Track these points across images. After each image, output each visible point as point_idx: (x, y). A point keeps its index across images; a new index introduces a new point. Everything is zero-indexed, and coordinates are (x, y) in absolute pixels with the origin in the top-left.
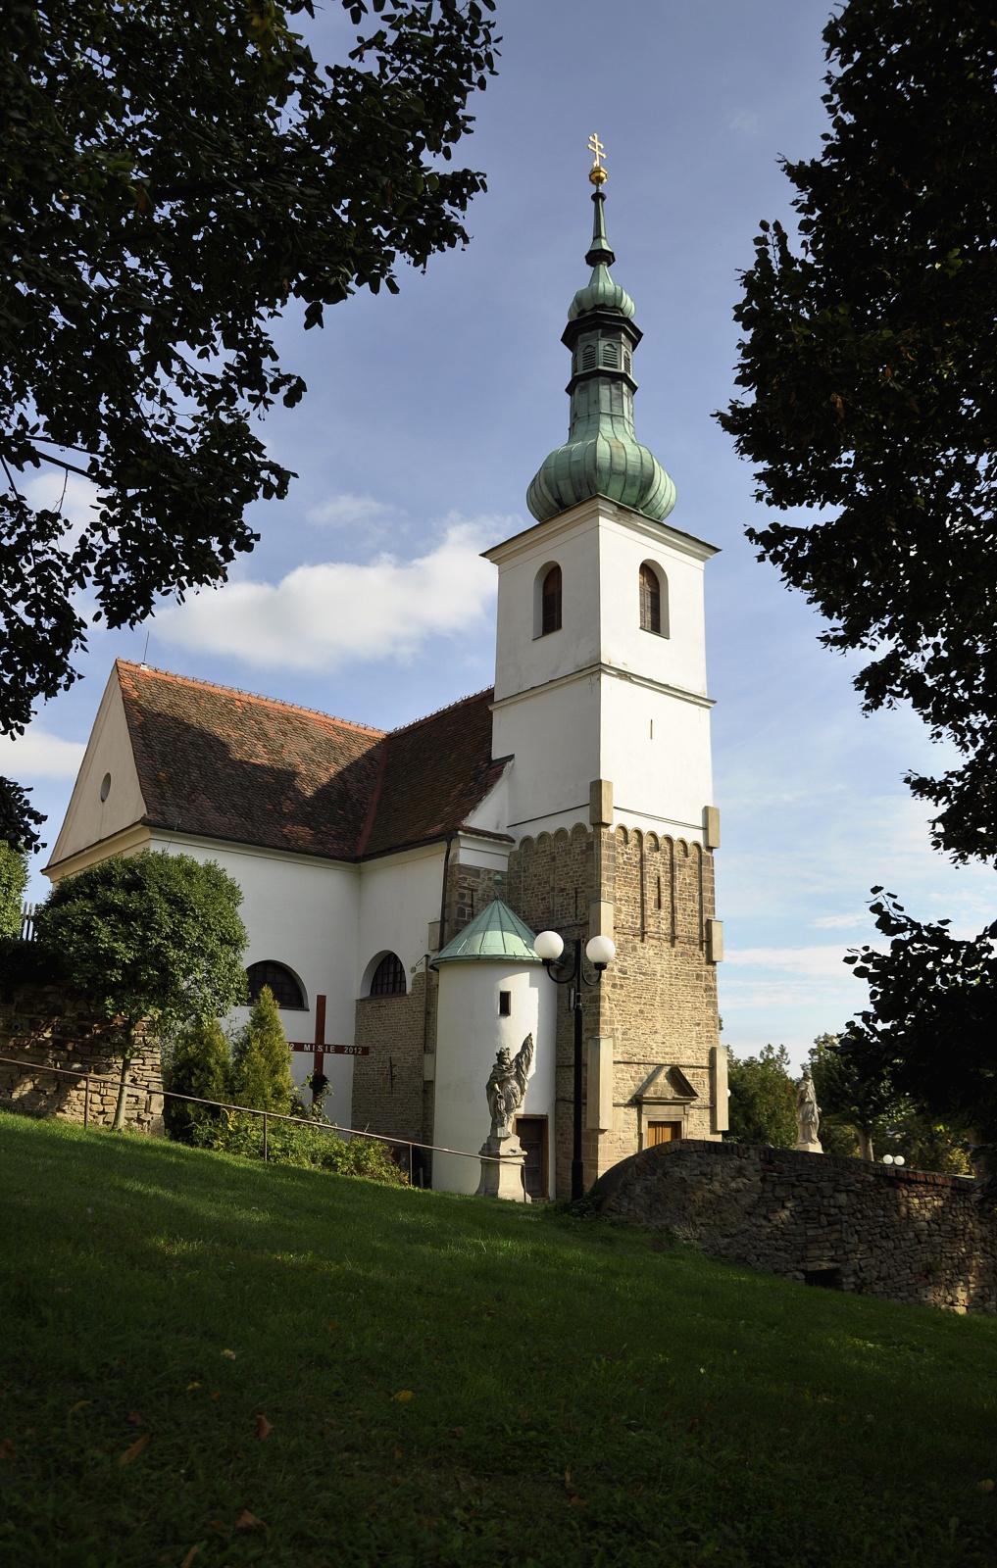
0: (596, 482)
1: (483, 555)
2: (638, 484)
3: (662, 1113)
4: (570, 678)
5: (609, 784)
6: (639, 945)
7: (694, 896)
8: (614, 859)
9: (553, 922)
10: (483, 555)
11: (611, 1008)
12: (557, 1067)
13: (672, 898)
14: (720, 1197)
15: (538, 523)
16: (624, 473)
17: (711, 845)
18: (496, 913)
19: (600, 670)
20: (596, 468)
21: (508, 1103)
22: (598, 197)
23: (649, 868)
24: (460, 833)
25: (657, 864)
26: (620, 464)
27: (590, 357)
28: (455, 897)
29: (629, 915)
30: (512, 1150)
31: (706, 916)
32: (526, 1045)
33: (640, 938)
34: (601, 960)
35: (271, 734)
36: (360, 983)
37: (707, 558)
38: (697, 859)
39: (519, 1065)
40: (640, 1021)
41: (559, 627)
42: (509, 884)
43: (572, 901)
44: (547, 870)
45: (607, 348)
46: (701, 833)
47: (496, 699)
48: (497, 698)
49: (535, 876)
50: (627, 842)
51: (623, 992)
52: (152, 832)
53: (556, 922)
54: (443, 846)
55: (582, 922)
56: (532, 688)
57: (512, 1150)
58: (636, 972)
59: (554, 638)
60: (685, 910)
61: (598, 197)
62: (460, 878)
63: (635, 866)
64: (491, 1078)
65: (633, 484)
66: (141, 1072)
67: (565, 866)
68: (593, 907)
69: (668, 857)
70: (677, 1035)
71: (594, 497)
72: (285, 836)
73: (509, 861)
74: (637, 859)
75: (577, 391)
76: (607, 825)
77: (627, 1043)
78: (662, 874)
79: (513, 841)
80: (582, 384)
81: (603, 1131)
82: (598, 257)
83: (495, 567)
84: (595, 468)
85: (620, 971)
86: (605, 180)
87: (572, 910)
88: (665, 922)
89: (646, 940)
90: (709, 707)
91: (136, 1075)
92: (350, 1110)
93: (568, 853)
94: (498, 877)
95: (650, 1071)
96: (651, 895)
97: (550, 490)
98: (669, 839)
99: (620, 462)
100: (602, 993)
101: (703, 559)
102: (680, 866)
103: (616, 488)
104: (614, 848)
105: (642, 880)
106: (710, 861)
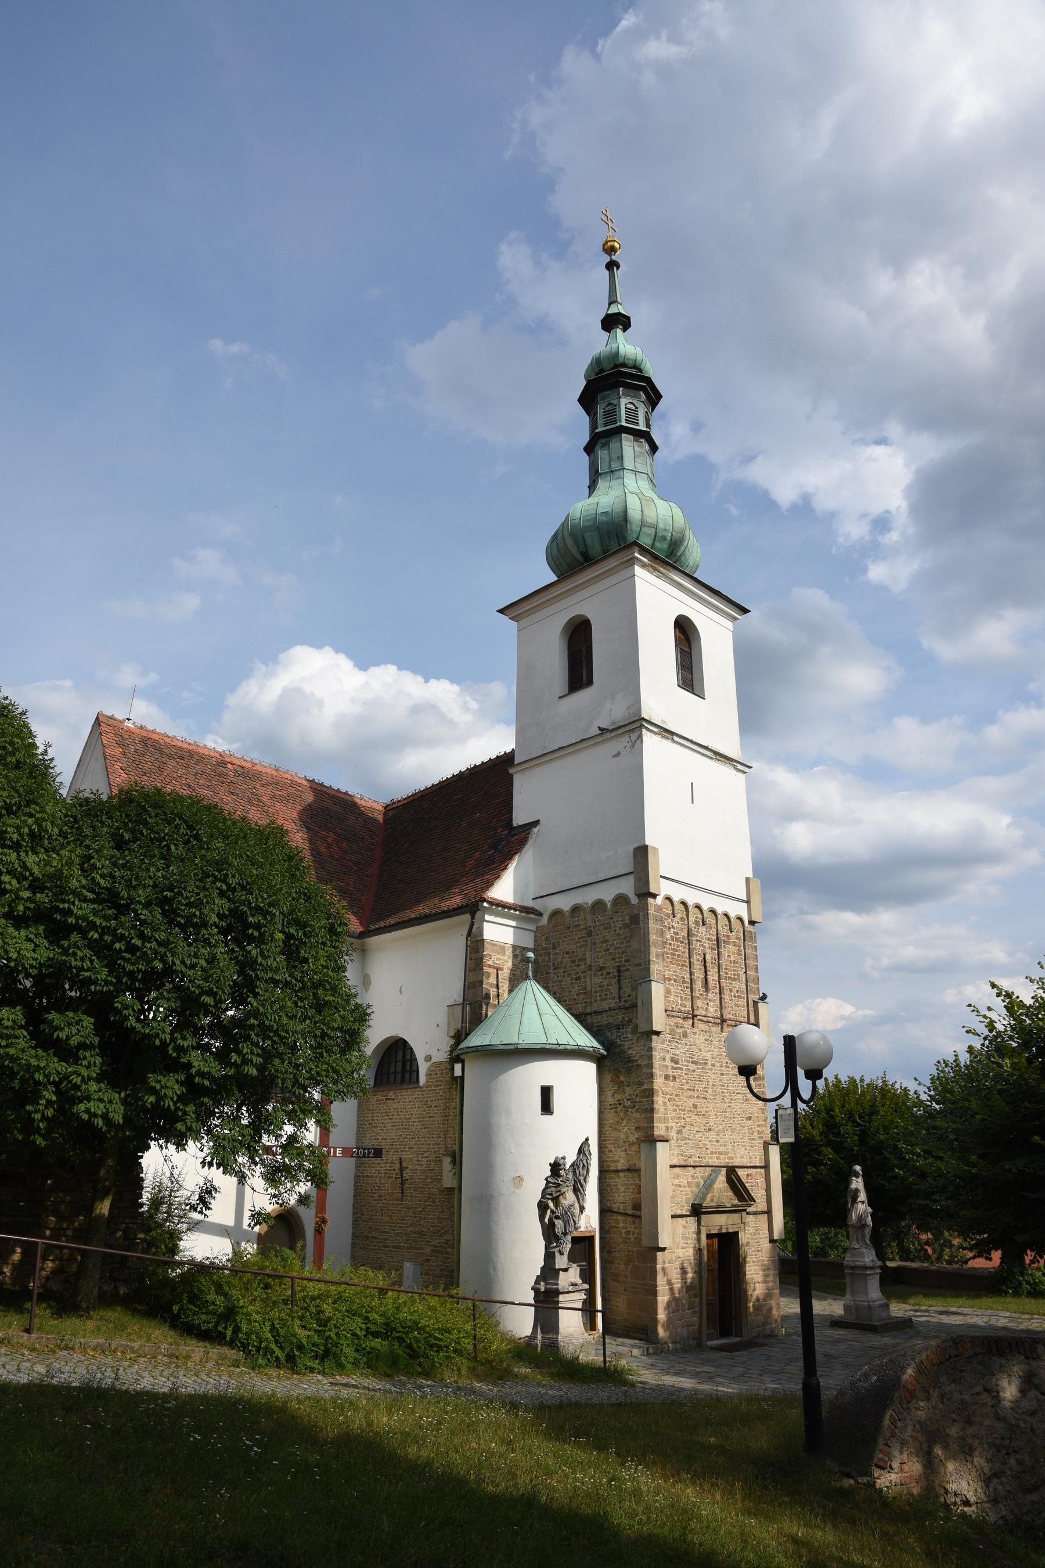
1: (501, 611)
5: (655, 849)
7: (739, 975)
10: (501, 611)
11: (665, 1103)
17: (753, 919)
19: (642, 726)
22: (612, 266)
26: (650, 517)
27: (612, 413)
30: (573, 1285)
32: (583, 1150)
34: (816, 1067)
35: (265, 798)
40: (694, 1117)
41: (590, 682)
43: (614, 981)
44: (581, 947)
45: (629, 406)
48: (517, 761)
49: (568, 953)
51: (676, 1084)
53: (595, 1004)
54: (467, 917)
55: (627, 1005)
58: (688, 1061)
59: (583, 696)
60: (731, 990)
61: (612, 266)
63: (682, 942)
69: (713, 931)
73: (535, 936)
74: (685, 933)
78: (708, 951)
79: (540, 914)
80: (603, 441)
81: (663, 1249)
82: (614, 322)
85: (673, 1060)
87: (614, 990)
88: (712, 1004)
89: (696, 1024)
90: (745, 772)
92: (350, 1218)
95: (706, 1174)
96: (699, 975)
100: (655, 1087)
102: (725, 942)
104: (662, 921)
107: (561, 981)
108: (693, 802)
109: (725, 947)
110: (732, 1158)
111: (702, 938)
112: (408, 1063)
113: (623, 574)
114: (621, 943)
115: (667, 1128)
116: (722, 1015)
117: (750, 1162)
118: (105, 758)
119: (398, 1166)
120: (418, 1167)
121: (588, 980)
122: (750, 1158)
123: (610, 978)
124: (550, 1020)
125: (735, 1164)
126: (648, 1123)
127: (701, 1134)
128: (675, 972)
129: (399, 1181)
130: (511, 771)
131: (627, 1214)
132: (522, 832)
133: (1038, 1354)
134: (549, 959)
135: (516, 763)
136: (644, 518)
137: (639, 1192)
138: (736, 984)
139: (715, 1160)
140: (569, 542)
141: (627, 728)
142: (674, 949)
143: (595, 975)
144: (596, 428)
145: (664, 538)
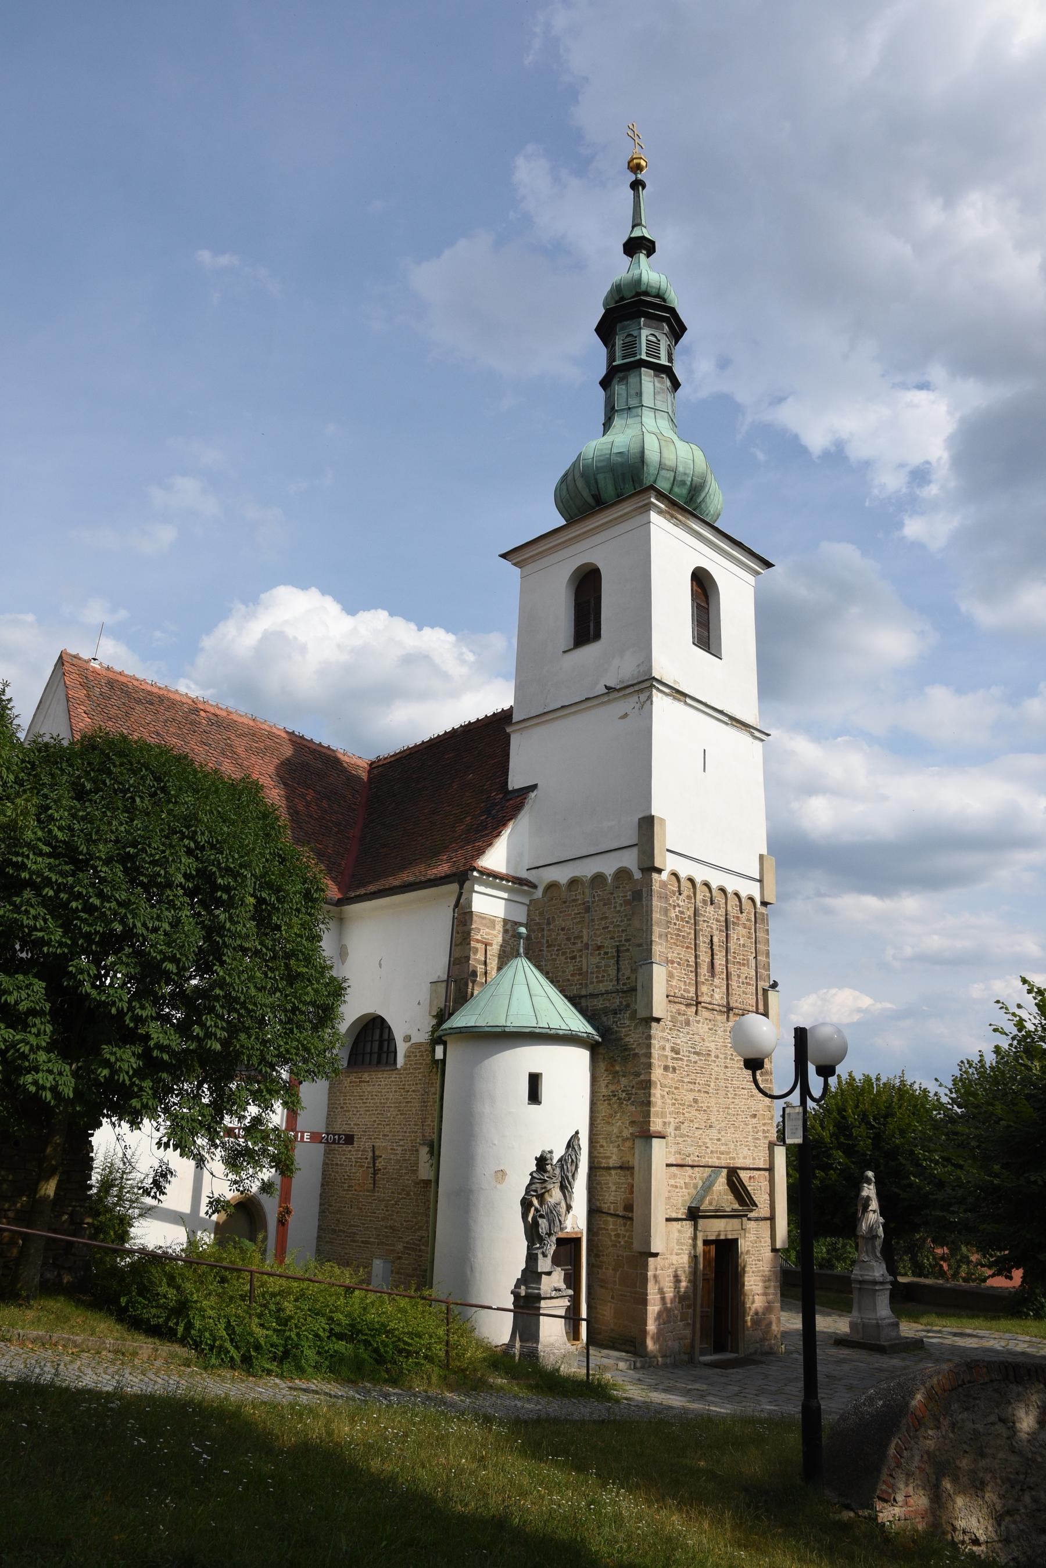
1: (504, 556)
3: (717, 1228)
7: (748, 960)
8: (666, 911)
10: (504, 556)
11: (663, 1097)
14: (1028, 1459)
18: (520, 974)
19: (652, 686)
22: (637, 185)
27: (631, 345)
32: (572, 1144)
35: (240, 750)
41: (597, 636)
44: (577, 923)
49: (563, 929)
54: (455, 887)
56: (563, 707)
57: (556, 1290)
59: (590, 651)
60: (739, 976)
61: (637, 185)
63: (687, 922)
67: (602, 919)
69: (722, 912)
73: (529, 910)
76: (659, 871)
77: (680, 1140)
79: (535, 887)
80: (621, 375)
81: (656, 1255)
82: (638, 246)
83: (517, 571)
85: (673, 1050)
87: (612, 972)
88: (718, 990)
89: (699, 1012)
90: (762, 740)
96: (705, 958)
97: (587, 483)
99: (670, 459)
100: (653, 1078)
107: (555, 960)
108: (704, 771)
110: (734, 1158)
111: (710, 919)
112: (386, 1044)
113: (639, 520)
116: (728, 1003)
117: (754, 1164)
118: (68, 701)
119: (370, 1154)
120: (392, 1156)
122: (754, 1159)
123: (608, 958)
124: (542, 1002)
127: (701, 1131)
128: (678, 954)
129: (371, 1170)
130: (508, 730)
131: (618, 1216)
134: (543, 935)
135: (514, 721)
136: (663, 460)
137: (632, 1192)
138: (744, 969)
140: (580, 484)
142: (679, 930)
143: (591, 954)
144: (614, 361)
145: (683, 483)
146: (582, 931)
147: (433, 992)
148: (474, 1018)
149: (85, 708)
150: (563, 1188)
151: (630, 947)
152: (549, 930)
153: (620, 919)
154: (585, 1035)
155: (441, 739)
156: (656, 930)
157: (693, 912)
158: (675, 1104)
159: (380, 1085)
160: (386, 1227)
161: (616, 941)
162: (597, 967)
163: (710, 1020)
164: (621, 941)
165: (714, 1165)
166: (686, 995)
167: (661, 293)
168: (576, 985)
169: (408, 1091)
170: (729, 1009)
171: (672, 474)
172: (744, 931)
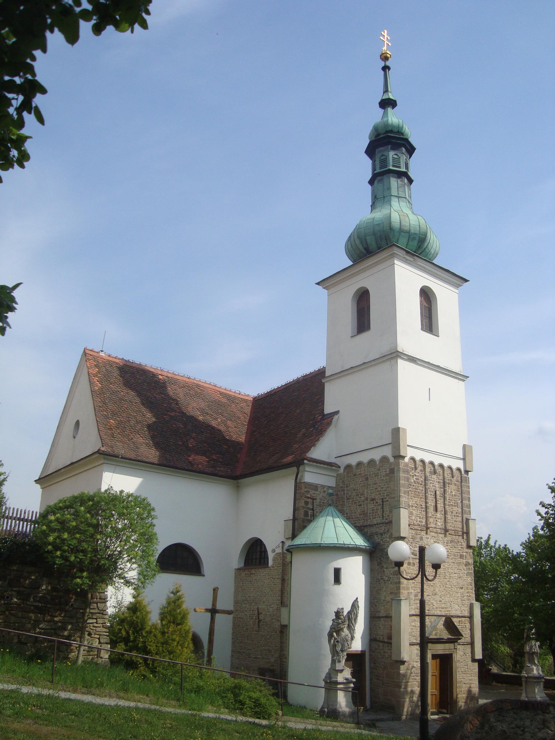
0: (391, 237)
1: (318, 284)
2: (417, 239)
4: (376, 362)
5: (405, 430)
6: (424, 536)
7: (457, 503)
8: (408, 479)
9: (367, 520)
10: (318, 284)
12: (370, 617)
13: (445, 504)
15: (352, 263)
16: (408, 232)
17: (468, 469)
20: (391, 229)
21: (343, 646)
22: (386, 68)
23: (430, 486)
24: (305, 461)
25: (435, 483)
27: (384, 162)
28: (302, 504)
29: (418, 516)
31: (465, 516)
32: (355, 606)
33: (425, 532)
36: (238, 559)
37: (460, 286)
38: (459, 479)
39: (349, 619)
42: (337, 495)
43: (380, 507)
46: (461, 462)
47: (327, 374)
49: (354, 490)
50: (416, 469)
52: (105, 459)
54: (294, 469)
55: (387, 521)
56: (351, 368)
59: (365, 336)
60: (452, 512)
61: (386, 68)
62: (305, 491)
63: (421, 484)
64: (331, 629)
65: (414, 239)
66: (95, 628)
68: (395, 511)
69: (441, 477)
70: (448, 596)
71: (391, 246)
72: (190, 462)
73: (337, 480)
75: (376, 182)
76: (403, 457)
78: (437, 489)
79: (339, 467)
80: (379, 178)
83: (326, 291)
84: (391, 229)
86: (390, 59)
87: (380, 512)
88: (440, 520)
91: (91, 631)
93: (377, 475)
94: (331, 491)
96: (431, 503)
97: (361, 242)
98: (441, 466)
99: (406, 224)
101: (457, 286)
103: (402, 242)
104: (408, 472)
105: (426, 493)
106: (467, 480)
107: (350, 506)
108: (429, 400)
109: (448, 487)
110: (450, 611)
111: (434, 481)
112: (263, 553)
113: (388, 263)
114: (384, 485)
115: (409, 593)
116: (445, 527)
117: (461, 614)
118: (89, 375)
119: (256, 613)
120: (267, 613)
121: (365, 506)
122: (462, 611)
123: (378, 506)
124: (341, 530)
125: (451, 615)
126: (397, 590)
127: (430, 597)
128: (416, 502)
129: (257, 621)
130: (323, 381)
132: (329, 418)
133: (550, 711)
134: (344, 493)
135: (326, 375)
136: (402, 227)
137: (391, 629)
138: (455, 509)
139: (438, 612)
140: (357, 242)
141: (389, 357)
142: (416, 489)
143: (369, 503)
144: (375, 170)
145: (414, 239)
146: (364, 491)
147: (286, 526)
148: (304, 540)
149: (98, 379)
150: (349, 627)
151: (389, 499)
152: (347, 490)
153: (383, 484)
154: (364, 547)
155: (291, 384)
156: (402, 489)
157: (424, 478)
158: (414, 583)
159: (260, 576)
160: (266, 650)
161: (381, 496)
162: (372, 510)
163: (435, 537)
164: (384, 496)
165: (437, 614)
166: (420, 524)
167: (400, 131)
168: (362, 520)
169: (275, 579)
170: (446, 531)
171: (408, 234)
172: (455, 487)
